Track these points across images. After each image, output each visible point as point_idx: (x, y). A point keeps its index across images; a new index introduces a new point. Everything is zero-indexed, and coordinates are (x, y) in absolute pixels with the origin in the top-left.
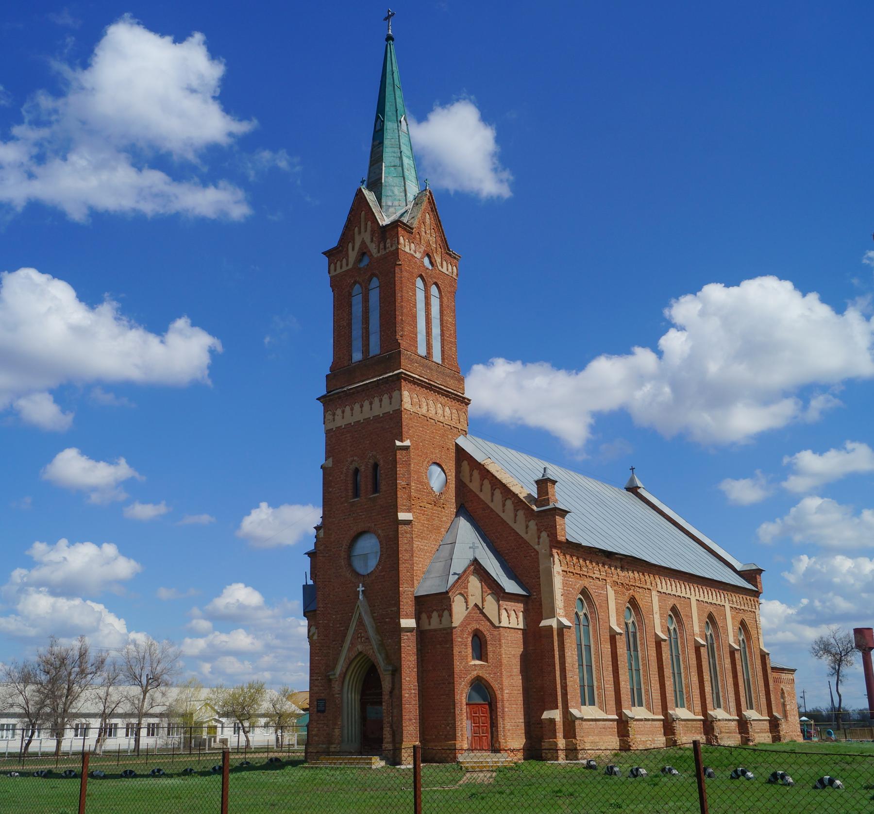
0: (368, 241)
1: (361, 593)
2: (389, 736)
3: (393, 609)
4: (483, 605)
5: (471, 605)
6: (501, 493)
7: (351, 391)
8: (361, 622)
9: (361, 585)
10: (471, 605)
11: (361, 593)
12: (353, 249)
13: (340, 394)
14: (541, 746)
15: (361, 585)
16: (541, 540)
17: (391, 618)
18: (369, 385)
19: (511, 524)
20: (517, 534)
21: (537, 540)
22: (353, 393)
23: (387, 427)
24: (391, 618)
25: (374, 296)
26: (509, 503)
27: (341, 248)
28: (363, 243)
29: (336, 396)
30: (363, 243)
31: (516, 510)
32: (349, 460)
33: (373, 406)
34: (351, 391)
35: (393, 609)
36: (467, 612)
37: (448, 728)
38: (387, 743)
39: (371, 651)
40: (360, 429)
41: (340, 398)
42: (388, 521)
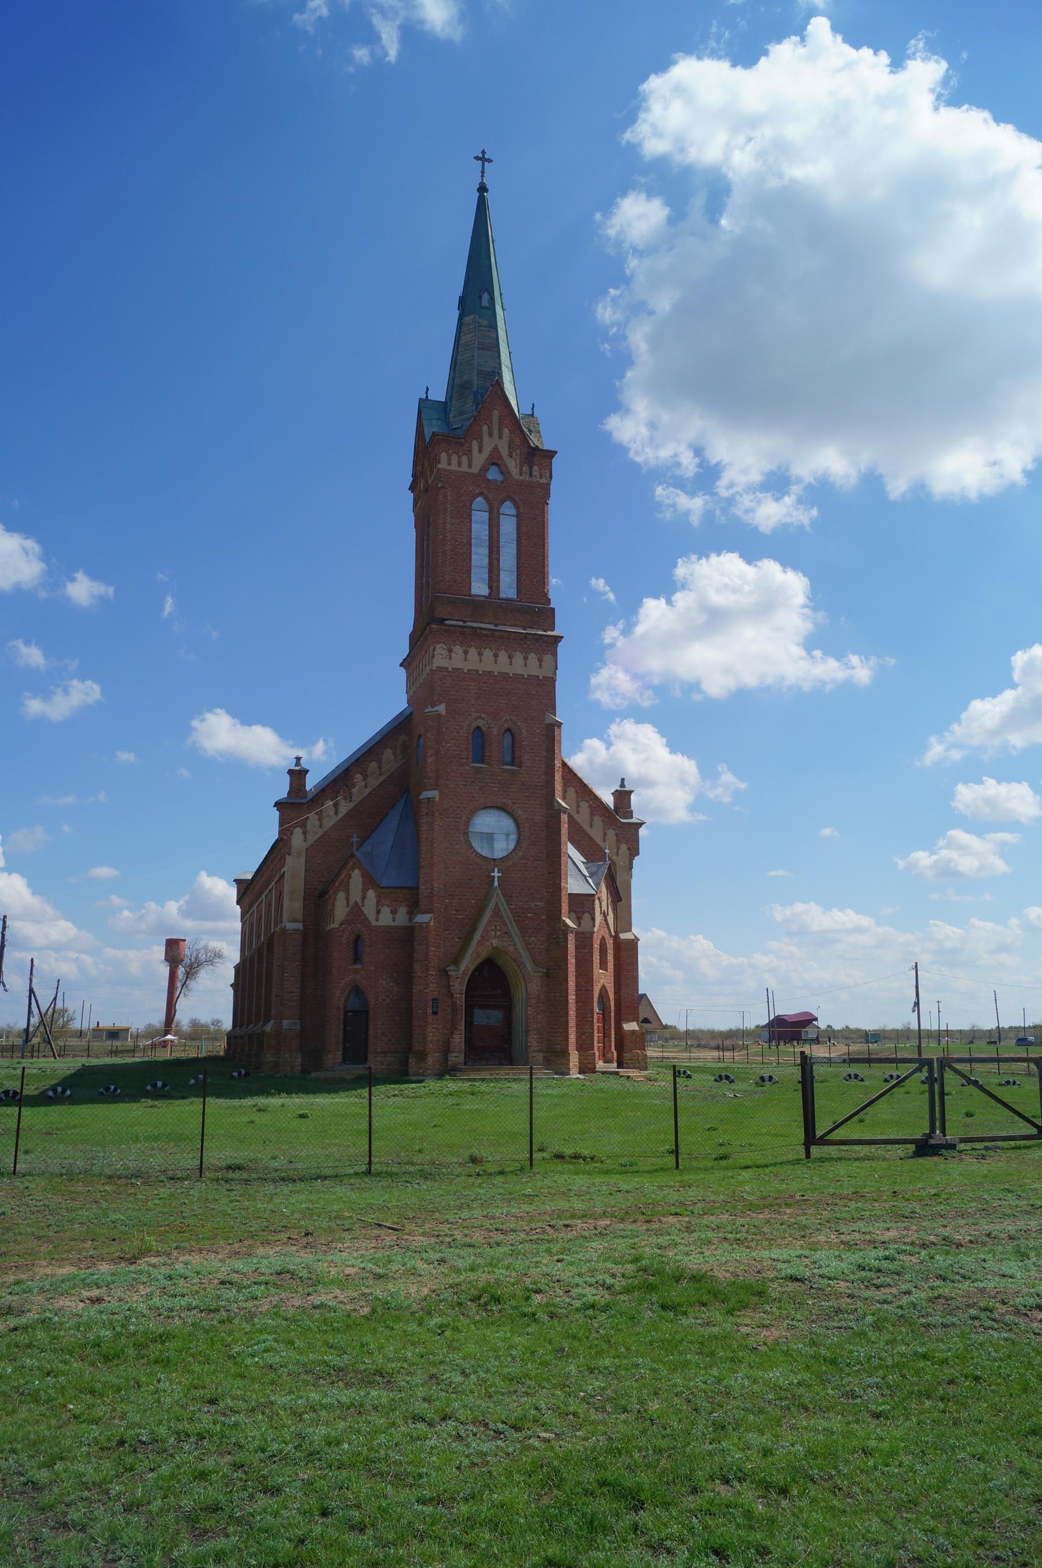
0: (504, 451)
1: (496, 879)
2: (536, 1044)
3: (539, 904)
4: (363, 902)
5: (352, 903)
6: (576, 792)
7: (484, 632)
8: (497, 913)
9: (496, 869)
10: (352, 903)
11: (496, 879)
12: (480, 451)
13: (465, 629)
14: (935, 1031)
15: (496, 869)
16: (620, 851)
17: (536, 914)
18: (513, 635)
19: (586, 827)
20: (592, 840)
21: (615, 850)
22: (485, 635)
23: (534, 693)
24: (536, 914)
25: (508, 527)
26: (584, 805)
27: (463, 440)
28: (496, 449)
29: (458, 629)
30: (496, 449)
31: (592, 814)
32: (474, 715)
33: (513, 660)
34: (484, 632)
35: (539, 904)
36: (348, 910)
37: (584, 1037)
38: (535, 1051)
39: (512, 948)
40: (491, 682)
41: (462, 633)
42: (532, 802)
